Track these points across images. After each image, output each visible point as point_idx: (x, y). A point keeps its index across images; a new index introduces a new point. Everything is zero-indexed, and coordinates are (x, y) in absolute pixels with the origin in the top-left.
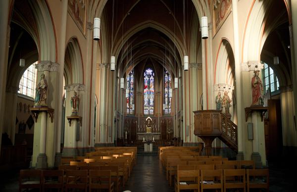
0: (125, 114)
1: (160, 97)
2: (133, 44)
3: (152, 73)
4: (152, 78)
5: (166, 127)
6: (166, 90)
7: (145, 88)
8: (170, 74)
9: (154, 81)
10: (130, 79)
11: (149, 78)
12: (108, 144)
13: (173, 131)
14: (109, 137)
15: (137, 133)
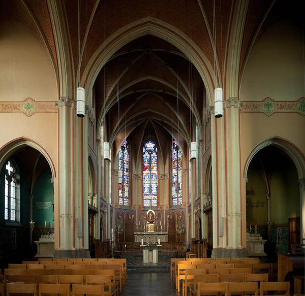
0: (116, 205)
1: (167, 181)
2: (121, 85)
3: (155, 147)
4: (154, 155)
5: (174, 224)
6: (174, 172)
7: (144, 169)
8: (180, 147)
9: (158, 160)
10: (123, 156)
11: (150, 155)
12: (76, 251)
13: (185, 229)
14: (77, 239)
15: (135, 233)
